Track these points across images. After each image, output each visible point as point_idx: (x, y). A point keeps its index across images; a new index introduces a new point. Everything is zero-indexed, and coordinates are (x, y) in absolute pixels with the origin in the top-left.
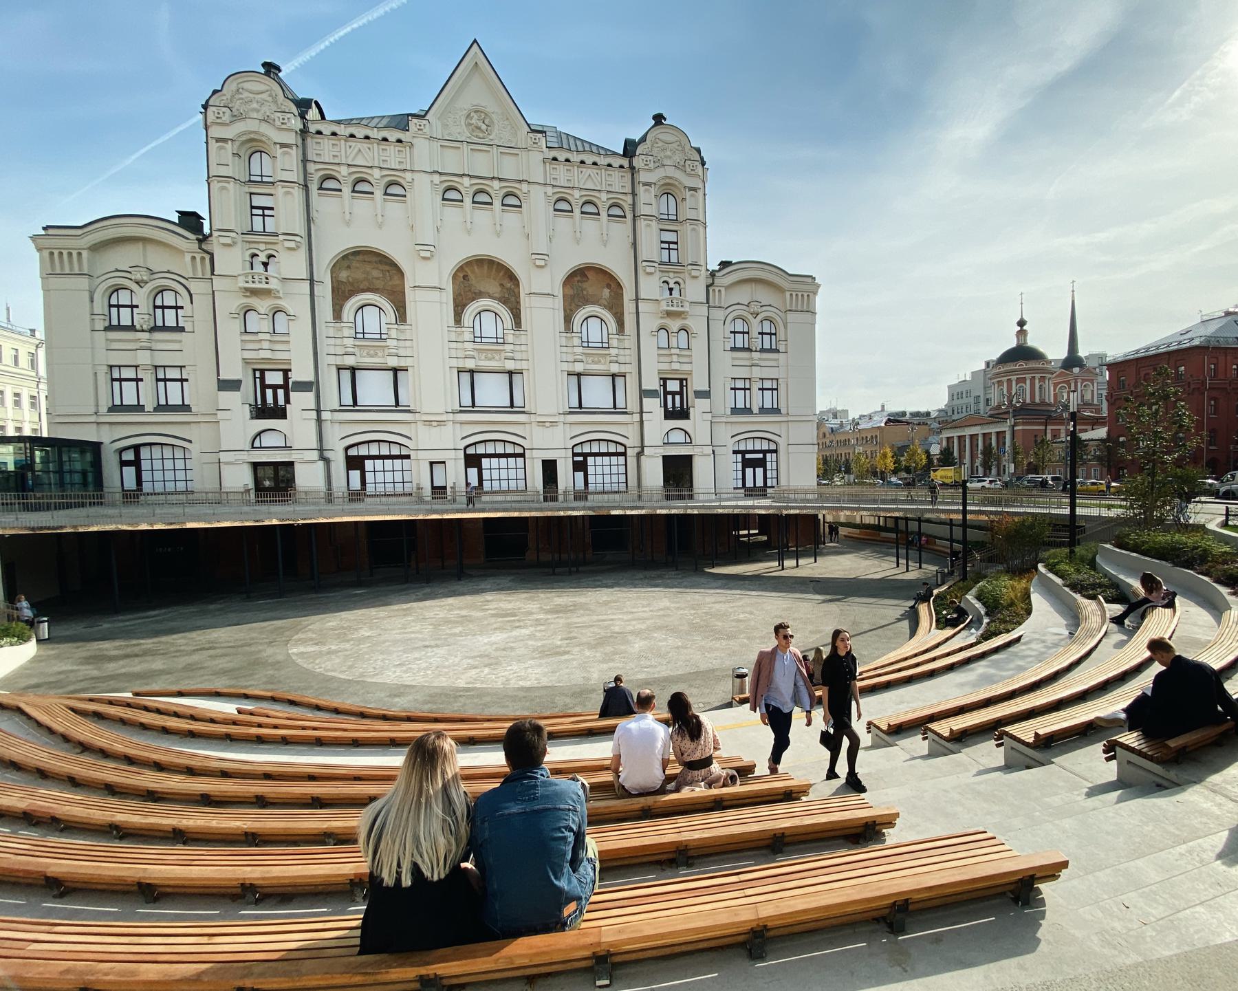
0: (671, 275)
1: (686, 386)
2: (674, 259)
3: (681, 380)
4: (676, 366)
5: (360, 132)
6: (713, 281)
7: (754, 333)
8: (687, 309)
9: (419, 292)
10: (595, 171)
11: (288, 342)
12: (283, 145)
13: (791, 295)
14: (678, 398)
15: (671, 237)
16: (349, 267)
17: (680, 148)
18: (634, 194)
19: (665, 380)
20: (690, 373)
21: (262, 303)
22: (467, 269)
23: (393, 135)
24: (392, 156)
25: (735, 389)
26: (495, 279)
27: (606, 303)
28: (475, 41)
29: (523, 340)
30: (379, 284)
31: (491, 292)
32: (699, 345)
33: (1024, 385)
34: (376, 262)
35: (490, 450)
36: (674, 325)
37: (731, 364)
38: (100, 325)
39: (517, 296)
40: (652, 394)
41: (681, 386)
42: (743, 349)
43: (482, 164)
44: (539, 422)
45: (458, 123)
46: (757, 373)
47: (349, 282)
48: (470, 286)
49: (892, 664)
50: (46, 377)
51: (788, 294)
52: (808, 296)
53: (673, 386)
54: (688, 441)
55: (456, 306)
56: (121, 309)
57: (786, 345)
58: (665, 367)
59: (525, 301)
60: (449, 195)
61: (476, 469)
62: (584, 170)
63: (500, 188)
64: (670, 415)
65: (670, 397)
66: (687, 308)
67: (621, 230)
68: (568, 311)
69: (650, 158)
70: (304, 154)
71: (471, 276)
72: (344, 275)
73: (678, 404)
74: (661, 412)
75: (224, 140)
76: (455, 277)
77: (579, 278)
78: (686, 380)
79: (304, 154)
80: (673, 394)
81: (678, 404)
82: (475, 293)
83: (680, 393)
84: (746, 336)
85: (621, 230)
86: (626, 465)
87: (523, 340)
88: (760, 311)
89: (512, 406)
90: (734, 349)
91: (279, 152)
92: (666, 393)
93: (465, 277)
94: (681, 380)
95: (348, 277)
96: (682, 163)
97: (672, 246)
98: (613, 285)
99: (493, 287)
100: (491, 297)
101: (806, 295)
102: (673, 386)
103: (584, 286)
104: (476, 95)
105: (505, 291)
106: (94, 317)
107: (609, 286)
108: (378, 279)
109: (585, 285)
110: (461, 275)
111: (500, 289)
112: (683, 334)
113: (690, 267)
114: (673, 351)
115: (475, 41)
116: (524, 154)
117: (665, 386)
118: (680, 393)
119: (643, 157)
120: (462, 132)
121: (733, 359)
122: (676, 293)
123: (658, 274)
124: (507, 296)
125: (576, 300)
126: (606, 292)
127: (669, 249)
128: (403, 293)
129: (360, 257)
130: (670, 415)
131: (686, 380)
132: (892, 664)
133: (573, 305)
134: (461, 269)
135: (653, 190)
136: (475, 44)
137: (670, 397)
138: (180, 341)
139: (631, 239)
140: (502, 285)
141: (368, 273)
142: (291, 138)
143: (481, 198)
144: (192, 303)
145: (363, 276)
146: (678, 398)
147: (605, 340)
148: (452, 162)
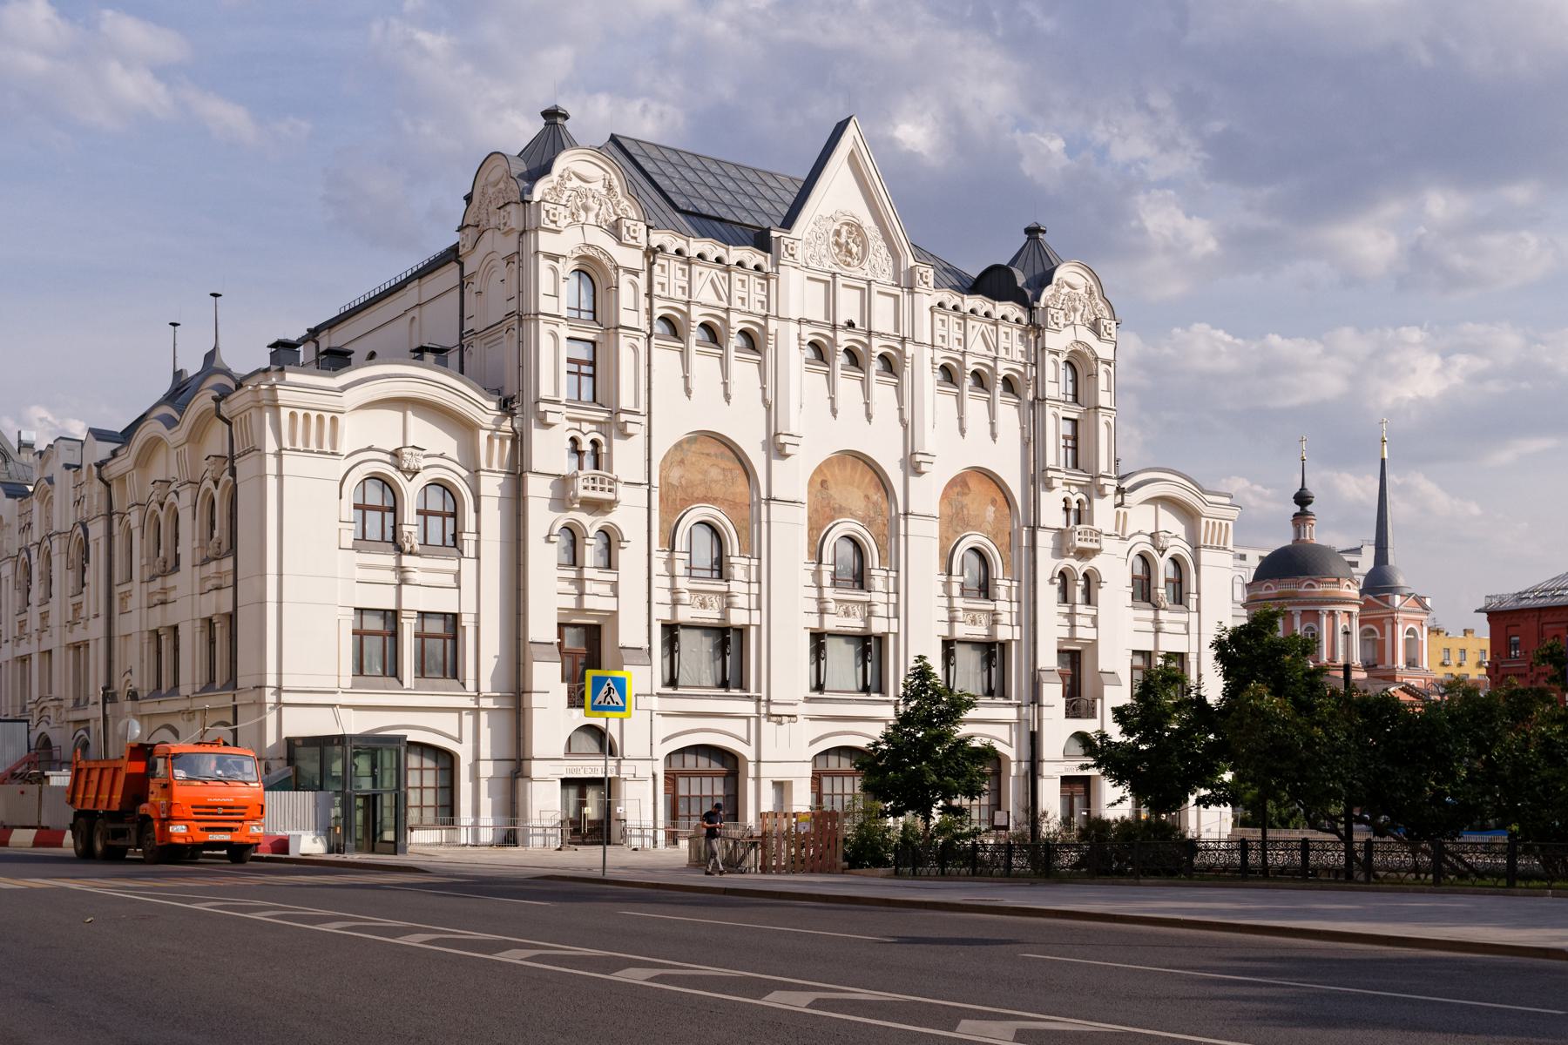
6: (1123, 499)
13: (293, 415)
16: (682, 462)
21: (592, 519)
22: (825, 471)
26: (858, 487)
27: (989, 529)
30: (717, 490)
33: (1314, 625)
34: (716, 455)
37: (1441, 660)
47: (681, 486)
48: (830, 497)
49: (280, 575)
50: (748, 779)
52: (334, 419)
56: (429, 518)
67: (1008, 413)
68: (945, 540)
71: (831, 483)
72: (675, 475)
76: (945, 495)
77: (959, 489)
93: (823, 483)
95: (681, 477)
100: (853, 515)
101: (327, 416)
103: (965, 502)
105: (871, 506)
109: (966, 500)
124: (872, 515)
125: (954, 523)
132: (280, 575)
134: (819, 470)
140: (867, 497)
141: (705, 473)
144: (341, 498)
145: (700, 477)
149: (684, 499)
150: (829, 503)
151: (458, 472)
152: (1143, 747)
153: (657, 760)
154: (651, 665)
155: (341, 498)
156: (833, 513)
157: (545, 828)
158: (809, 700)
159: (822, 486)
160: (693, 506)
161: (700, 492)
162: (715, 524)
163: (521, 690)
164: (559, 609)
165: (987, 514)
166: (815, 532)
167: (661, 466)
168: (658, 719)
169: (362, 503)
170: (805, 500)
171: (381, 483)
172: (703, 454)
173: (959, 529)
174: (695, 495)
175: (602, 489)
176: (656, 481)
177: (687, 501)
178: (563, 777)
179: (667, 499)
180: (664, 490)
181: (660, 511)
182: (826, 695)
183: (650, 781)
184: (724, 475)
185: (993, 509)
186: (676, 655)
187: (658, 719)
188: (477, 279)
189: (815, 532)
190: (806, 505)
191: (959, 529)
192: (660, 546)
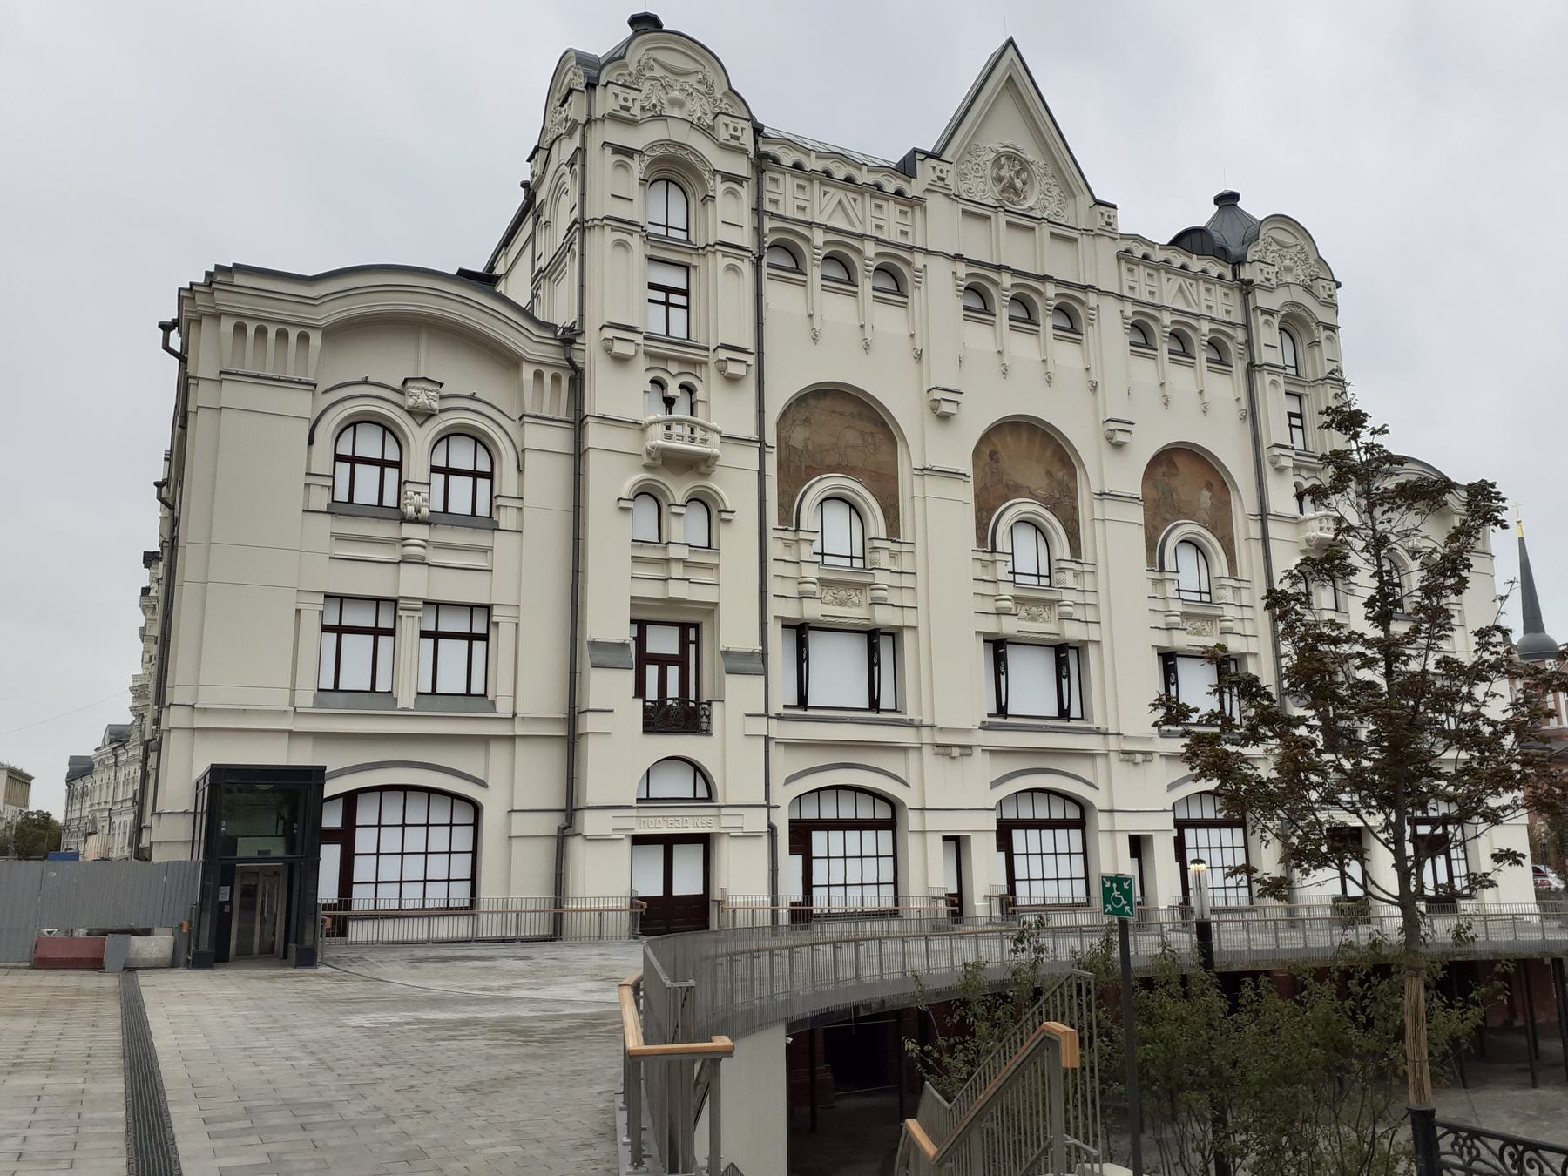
0: (674, 368)
1: (697, 643)
2: (678, 331)
3: (684, 628)
4: (677, 590)
5: (840, 172)
7: (418, 464)
8: (715, 451)
9: (933, 485)
10: (851, 195)
11: (714, 567)
12: (728, 177)
14: (673, 672)
15: (675, 279)
16: (807, 421)
17: (703, 89)
18: (1247, 327)
19: (641, 625)
20: (711, 609)
23: (891, 185)
24: (891, 223)
25: (436, 635)
28: (1011, 42)
29: (906, 563)
30: (855, 459)
31: (1033, 487)
32: (738, 543)
35: (829, 813)
36: (679, 490)
38: (320, 500)
39: (1072, 495)
40: (606, 654)
41: (684, 643)
42: (378, 511)
43: (1018, 252)
44: (938, 746)
45: (980, 174)
46: (413, 583)
51: (528, 372)
53: (663, 642)
54: (702, 792)
55: (979, 511)
56: (358, 467)
57: (520, 509)
58: (652, 591)
59: (907, 484)
60: (1141, 332)
61: (702, 846)
62: (832, 190)
63: (825, 243)
64: (659, 719)
65: (652, 671)
66: (713, 447)
68: (1152, 530)
69: (633, 94)
70: (759, 198)
71: (1003, 455)
72: (798, 436)
73: (673, 690)
74: (634, 711)
75: (628, 152)
76: (977, 453)
78: (697, 626)
79: (759, 198)
80: (663, 661)
81: (673, 690)
82: (1007, 486)
83: (681, 660)
84: (391, 474)
85: (1226, 389)
86: (475, 853)
87: (906, 563)
88: (436, 405)
89: (874, 704)
90: (335, 509)
91: (719, 187)
92: (643, 659)
93: (993, 455)
94: (684, 628)
96: (708, 120)
97: (674, 299)
98: (1216, 485)
99: (1035, 477)
100: (1032, 495)
102: (663, 642)
104: (1006, 132)
106: (312, 480)
107: (1209, 486)
108: (854, 447)
110: (986, 450)
111: (1046, 481)
112: (697, 516)
113: (723, 354)
114: (674, 552)
115: (1011, 42)
116: (1084, 242)
117: (641, 640)
118: (681, 660)
119: (618, 90)
120: (984, 190)
121: (340, 538)
122: (681, 411)
123: (642, 363)
124: (1057, 496)
126: (1206, 496)
127: (667, 304)
128: (894, 479)
129: (826, 404)
130: (659, 719)
131: (697, 626)
133: (1159, 519)
135: (637, 167)
136: (1011, 48)
137: (652, 671)
138: (484, 551)
139: (1244, 405)
140: (1049, 474)
142: (741, 167)
143: (1025, 311)
144: (311, 442)
146: (673, 672)
147: (1205, 588)
148: (977, 242)
149: (810, 466)
150: (1001, 480)
151: (488, 414)
152: (1374, 803)
153: (777, 807)
154: (765, 673)
155: (311, 442)
156: (1006, 491)
157: (1081, 927)
158: (985, 727)
159: (991, 459)
160: (824, 476)
161: (832, 459)
162: (1036, 520)
163: (577, 710)
164: (632, 597)
165: (1202, 500)
166: (985, 514)
167: (779, 424)
168: (777, 754)
169: (472, 469)
170: (970, 472)
171: (382, 429)
172: (834, 412)
173: (1168, 516)
174: (826, 462)
175: (693, 440)
176: (771, 438)
177: (814, 469)
178: (633, 833)
179: (789, 466)
180: (783, 455)
181: (779, 480)
182: (883, 715)
183: (765, 840)
184: (863, 438)
185: (1209, 494)
186: (876, 669)
187: (777, 754)
188: (546, 210)
189: (985, 514)
190: (971, 480)
191: (1168, 516)
192: (780, 524)
